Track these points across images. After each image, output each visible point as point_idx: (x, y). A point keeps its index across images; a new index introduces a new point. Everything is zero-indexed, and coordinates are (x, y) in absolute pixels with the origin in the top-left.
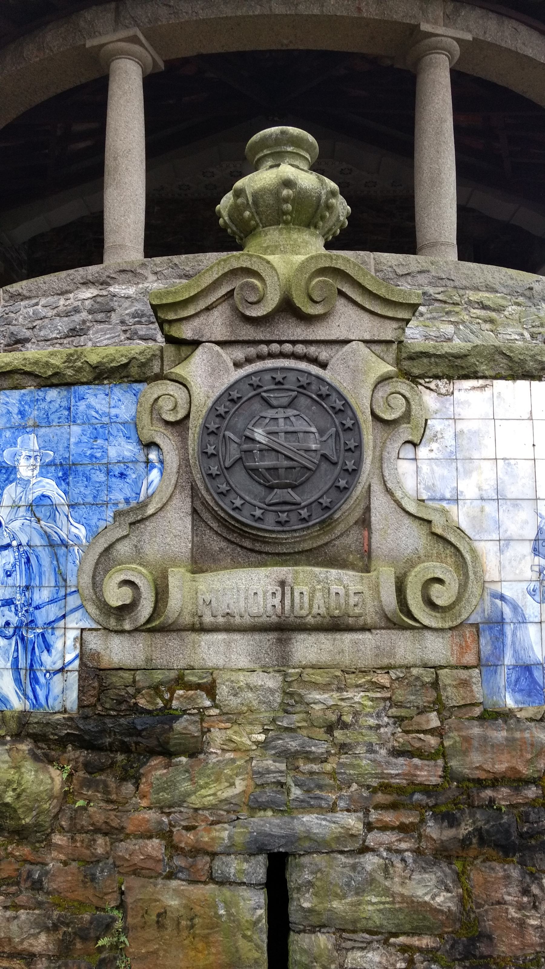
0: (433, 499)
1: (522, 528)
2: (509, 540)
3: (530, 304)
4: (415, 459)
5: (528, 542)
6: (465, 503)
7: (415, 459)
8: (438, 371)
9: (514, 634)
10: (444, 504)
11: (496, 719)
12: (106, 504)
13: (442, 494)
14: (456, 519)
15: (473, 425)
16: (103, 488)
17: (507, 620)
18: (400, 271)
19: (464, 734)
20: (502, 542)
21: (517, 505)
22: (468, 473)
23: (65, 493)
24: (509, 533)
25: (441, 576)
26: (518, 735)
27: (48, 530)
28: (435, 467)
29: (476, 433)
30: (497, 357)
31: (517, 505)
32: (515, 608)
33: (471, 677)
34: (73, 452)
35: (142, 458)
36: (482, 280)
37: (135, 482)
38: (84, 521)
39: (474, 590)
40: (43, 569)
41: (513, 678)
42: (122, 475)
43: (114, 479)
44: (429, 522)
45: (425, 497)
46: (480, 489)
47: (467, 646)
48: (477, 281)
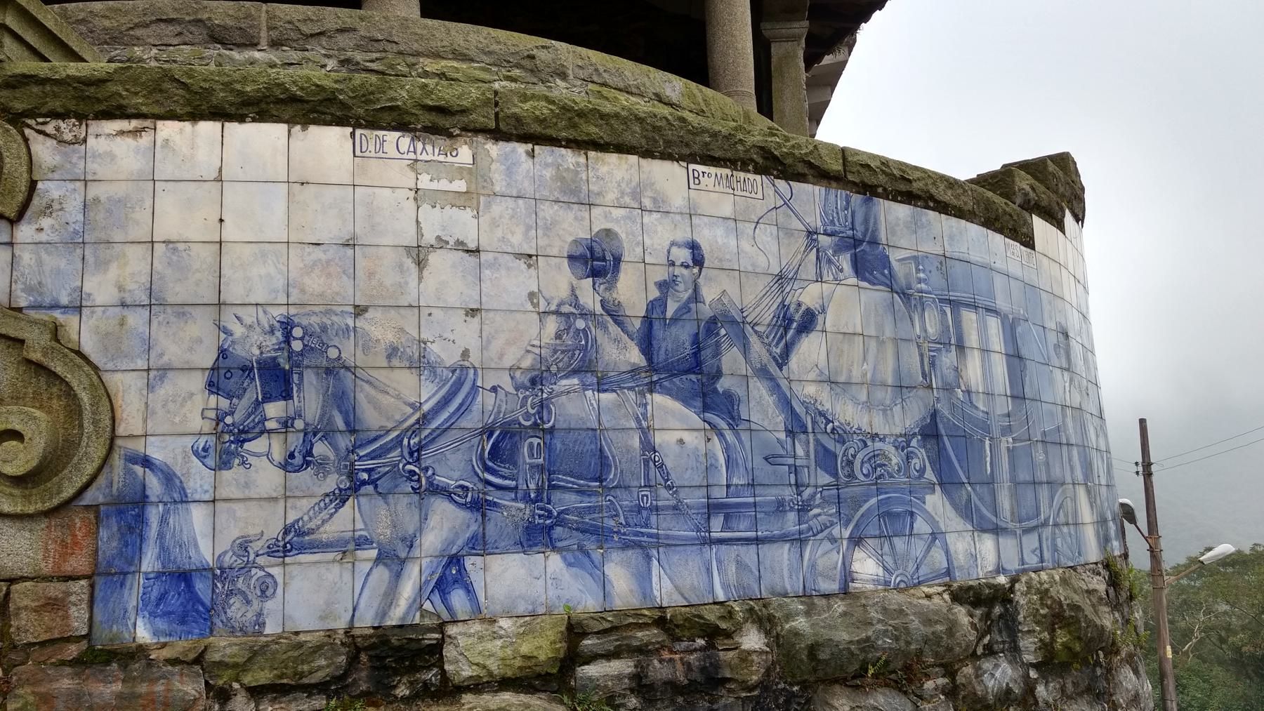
0: (37, 307)
1: (191, 349)
2: (165, 370)
3: (535, 80)
4: (11, 244)
5: (199, 373)
6: (93, 312)
7: (11, 244)
8: (56, 105)
9: (163, 521)
10: (57, 315)
11: (108, 663)
14: (75, 337)
15: (118, 190)
17: (153, 499)
18: (306, 29)
19: (42, 689)
20: (152, 374)
22: (102, 265)
24: (166, 358)
25: (18, 427)
26: (143, 688)
28: (44, 256)
29: (121, 202)
30: (167, 85)
31: (184, 314)
32: (169, 478)
33: (68, 594)
36: (445, 43)
39: (90, 450)
41: (155, 594)
44: (22, 342)
45: (23, 304)
46: (121, 289)
47: (76, 544)
48: (435, 45)
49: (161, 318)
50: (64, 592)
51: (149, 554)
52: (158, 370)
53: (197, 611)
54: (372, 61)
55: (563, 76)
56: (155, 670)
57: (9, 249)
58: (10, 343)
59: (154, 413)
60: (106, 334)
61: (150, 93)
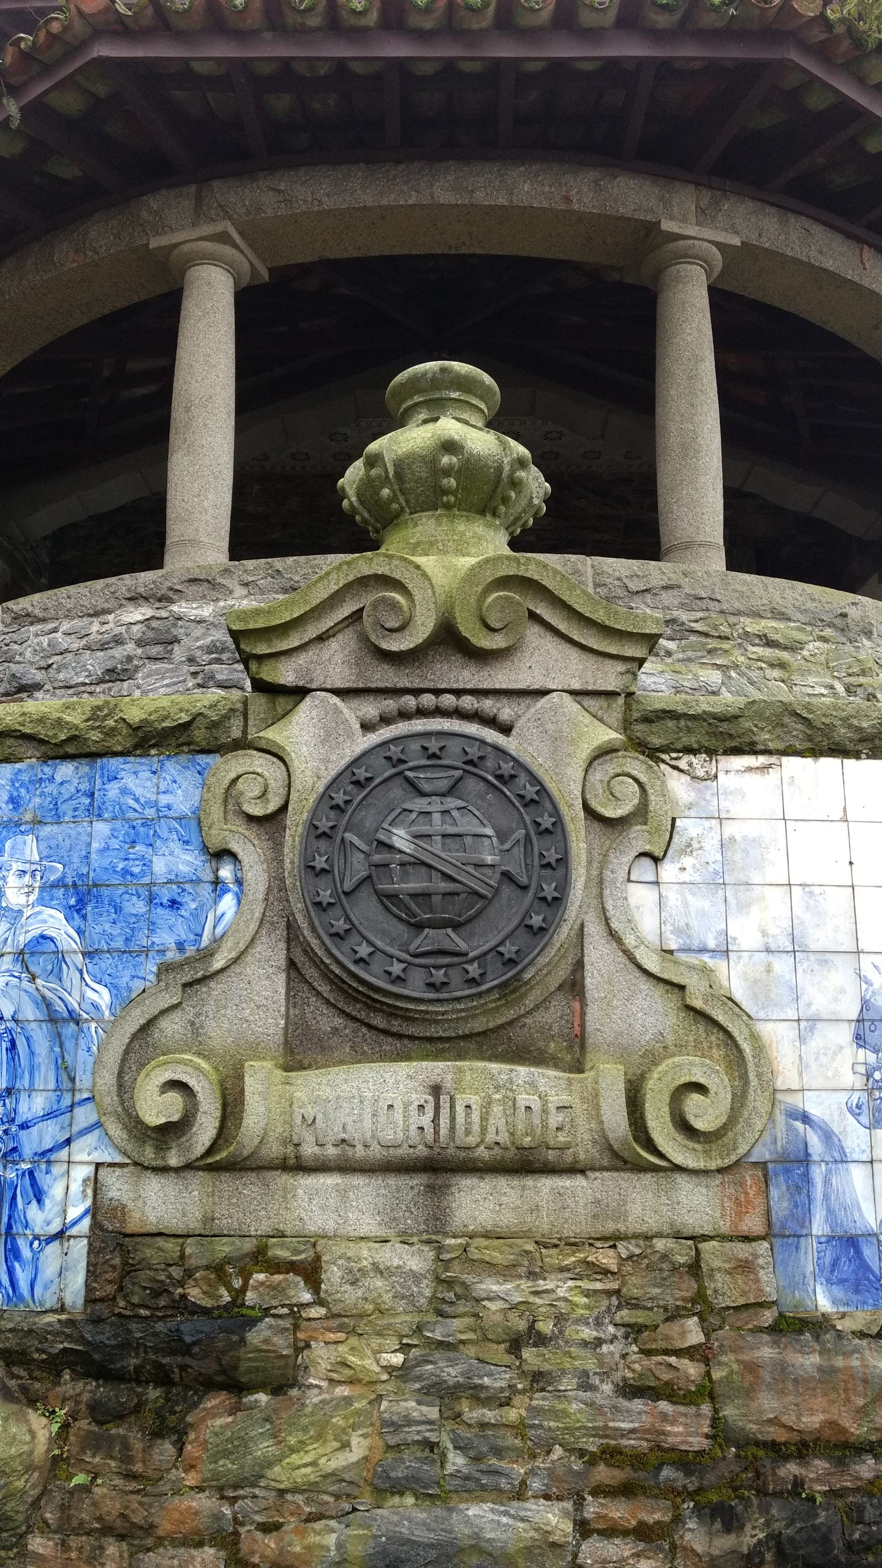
0: (688, 950)
1: (836, 1000)
2: (814, 1020)
3: (844, 640)
4: (657, 883)
5: (846, 1025)
6: (739, 958)
7: (657, 883)
8: (691, 740)
9: (827, 1181)
10: (706, 958)
11: (801, 1332)
12: (146, 951)
13: (701, 942)
14: (725, 983)
16: (143, 924)
17: (815, 1157)
18: (633, 586)
19: (746, 1357)
20: (803, 1024)
21: (826, 961)
22: (744, 907)
23: (79, 932)
24: (813, 1008)
25: (702, 1081)
27: (49, 994)
28: (690, 898)
30: (786, 720)
32: (828, 1136)
34: (95, 865)
35: (208, 876)
36: (765, 601)
37: (195, 915)
38: (108, 979)
40: (39, 1060)
41: (828, 1260)
42: (174, 904)
43: (160, 911)
44: (682, 988)
45: (673, 947)
46: (764, 934)
47: (748, 1202)
49: (805, 966)
50: (752, 1254)
51: (818, 1216)
52: (808, 1020)
53: (869, 1280)
54: (697, 621)
55: (868, 634)
56: (845, 1342)
57: (655, 887)
58: (668, 987)
59: (808, 1066)
60: (755, 980)
61: (774, 728)
